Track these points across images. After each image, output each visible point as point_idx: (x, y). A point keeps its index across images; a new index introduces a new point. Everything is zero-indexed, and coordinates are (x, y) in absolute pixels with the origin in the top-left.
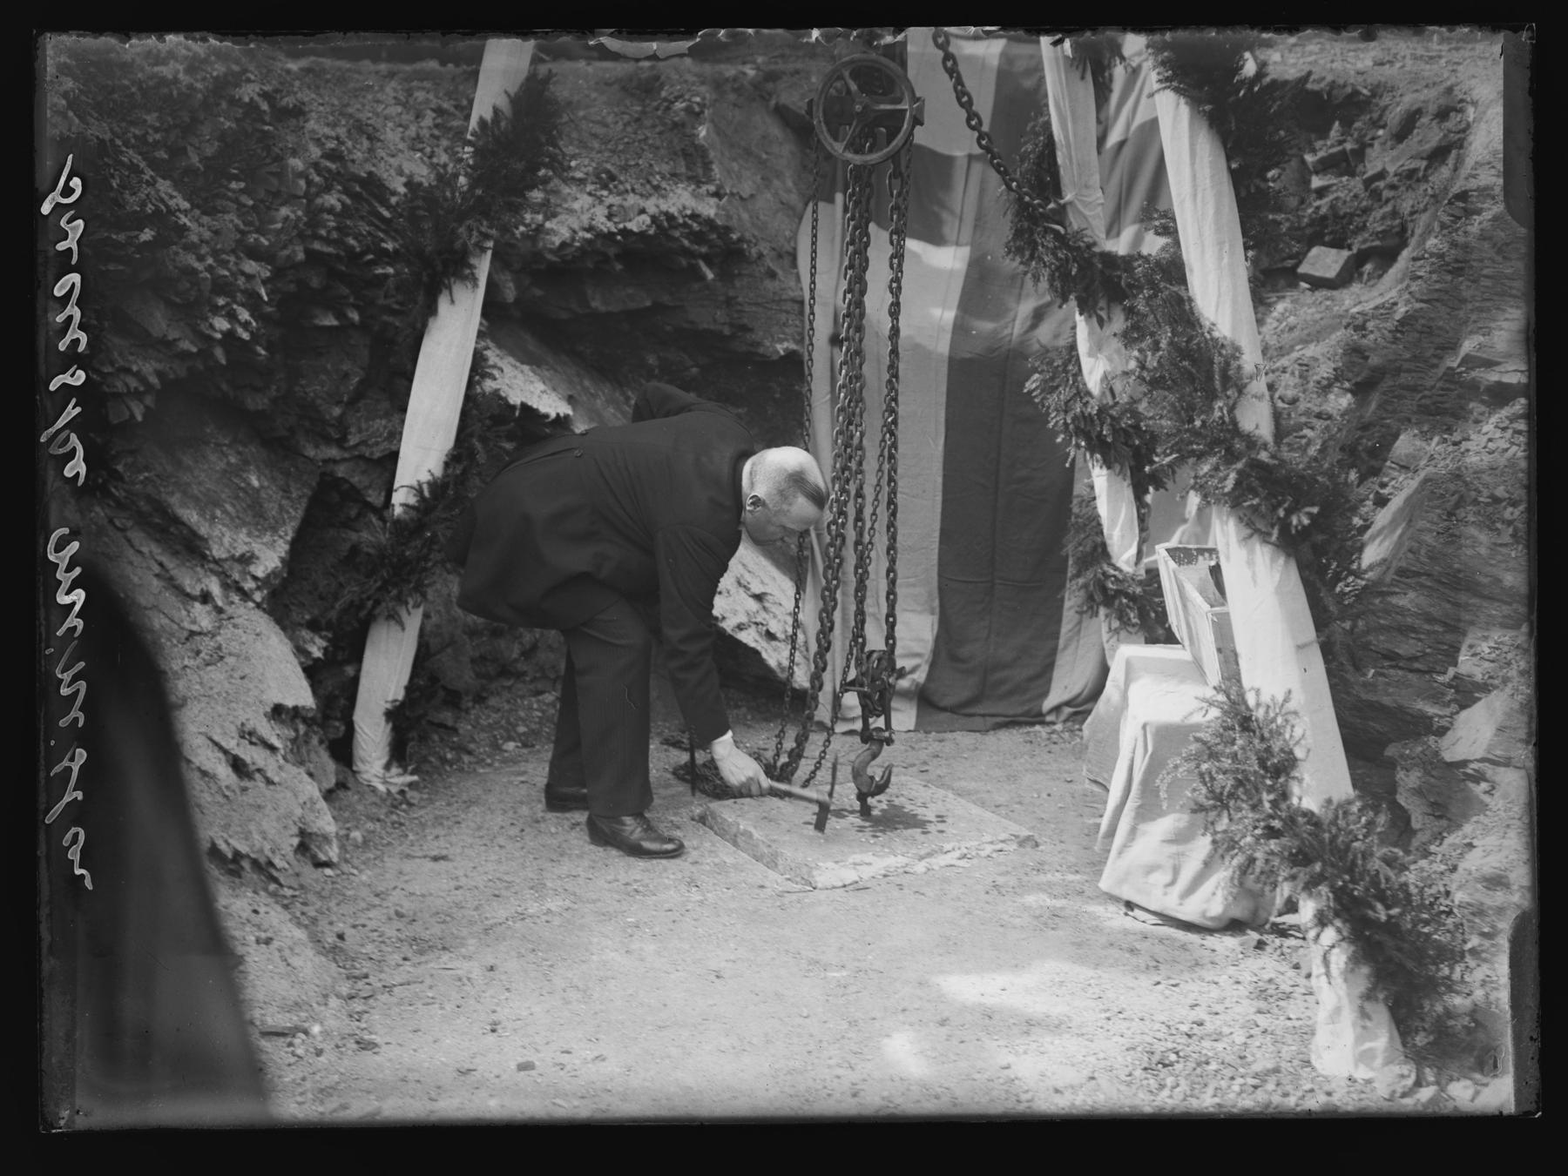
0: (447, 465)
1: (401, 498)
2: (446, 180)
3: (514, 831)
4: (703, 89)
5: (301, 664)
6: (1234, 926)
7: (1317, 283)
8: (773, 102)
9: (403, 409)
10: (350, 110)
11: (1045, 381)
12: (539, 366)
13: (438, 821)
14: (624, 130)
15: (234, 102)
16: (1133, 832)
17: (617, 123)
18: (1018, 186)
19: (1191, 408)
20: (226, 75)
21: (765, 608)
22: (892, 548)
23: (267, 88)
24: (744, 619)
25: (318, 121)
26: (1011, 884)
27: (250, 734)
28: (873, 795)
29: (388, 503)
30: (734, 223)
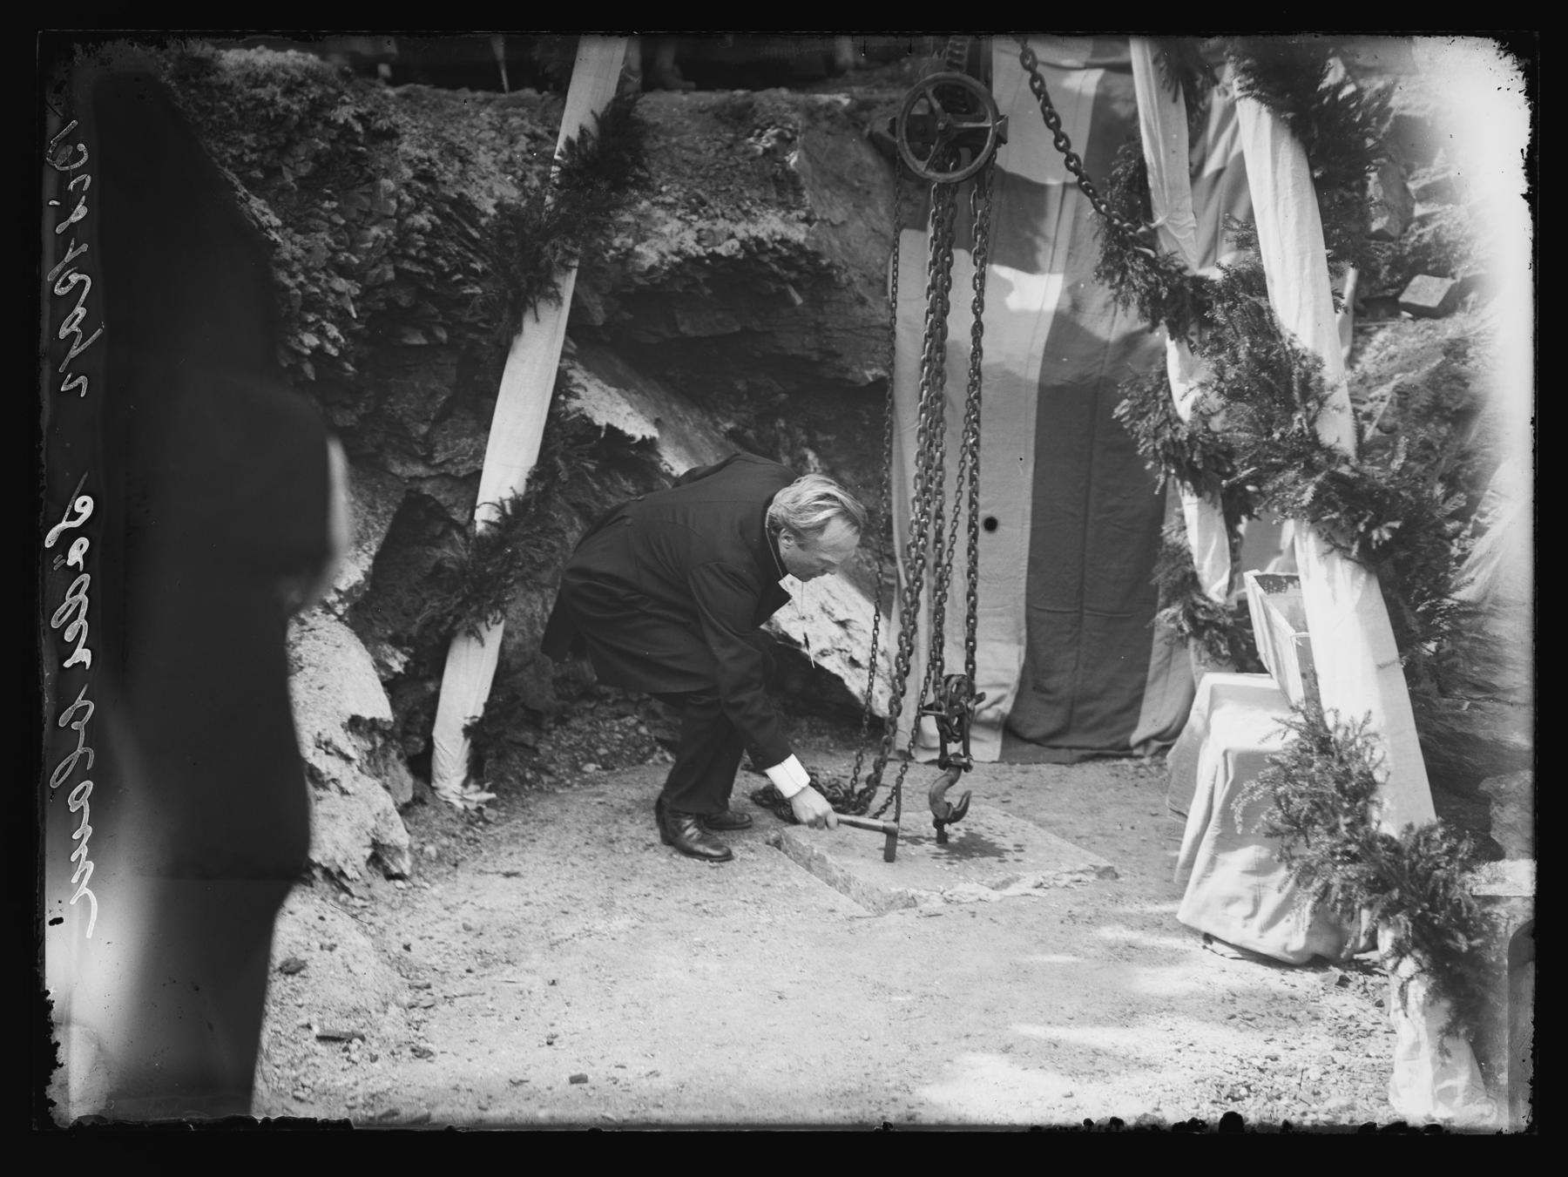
0: (529, 481)
1: (484, 515)
2: (536, 201)
3: (586, 850)
4: (795, 116)
5: (381, 678)
6: (1316, 962)
7: (1420, 313)
8: (867, 131)
9: (488, 428)
10: (444, 134)
11: (1134, 407)
12: (627, 390)
13: (513, 838)
14: (716, 156)
15: (329, 123)
16: (1213, 861)
17: (709, 149)
18: (1108, 209)
19: (1270, 420)
20: (321, 98)
21: (849, 635)
22: (972, 570)
23: (362, 110)
24: (827, 646)
25: (411, 143)
26: (1088, 914)
27: (327, 744)
28: (950, 822)
29: (472, 520)
30: (824, 248)
